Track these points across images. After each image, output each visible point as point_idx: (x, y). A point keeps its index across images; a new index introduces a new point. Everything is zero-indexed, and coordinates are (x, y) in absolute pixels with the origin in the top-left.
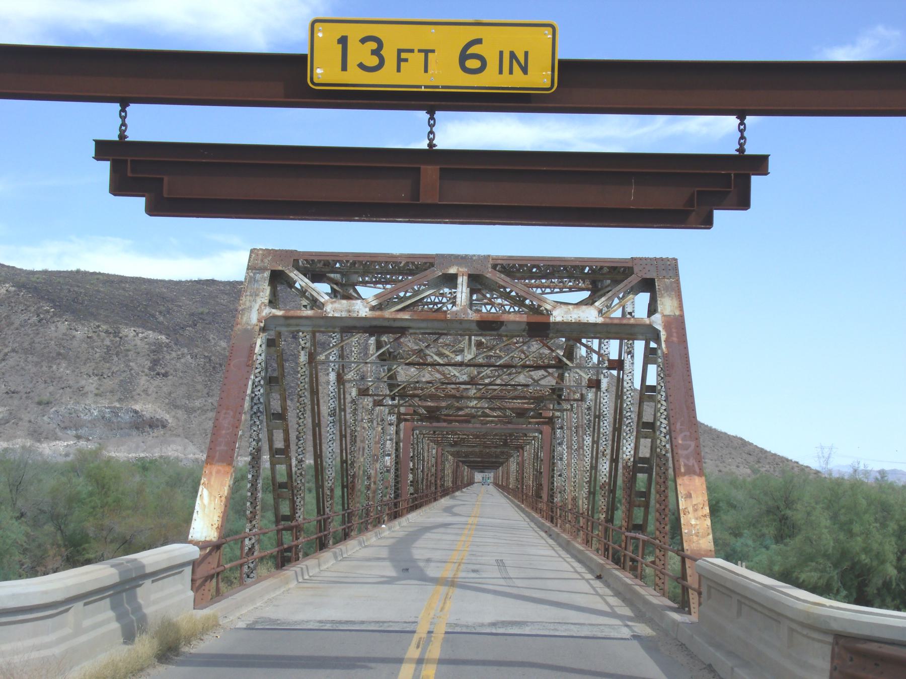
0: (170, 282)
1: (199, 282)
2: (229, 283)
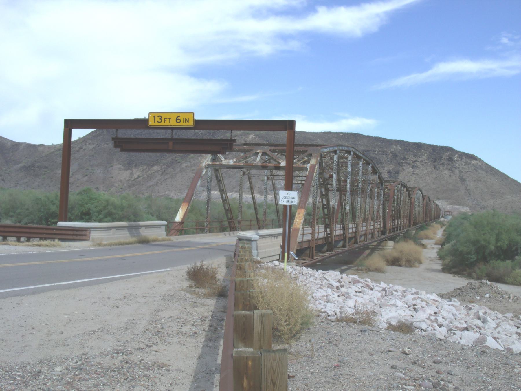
0: (314, 133)
1: (325, 133)
2: (337, 133)
